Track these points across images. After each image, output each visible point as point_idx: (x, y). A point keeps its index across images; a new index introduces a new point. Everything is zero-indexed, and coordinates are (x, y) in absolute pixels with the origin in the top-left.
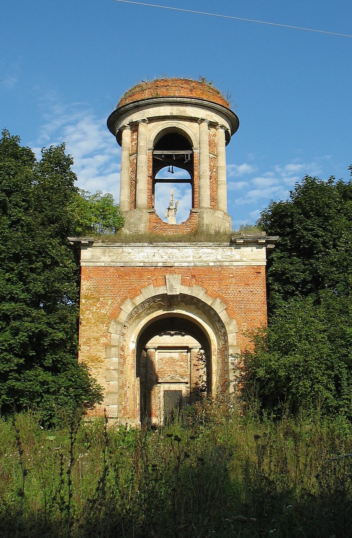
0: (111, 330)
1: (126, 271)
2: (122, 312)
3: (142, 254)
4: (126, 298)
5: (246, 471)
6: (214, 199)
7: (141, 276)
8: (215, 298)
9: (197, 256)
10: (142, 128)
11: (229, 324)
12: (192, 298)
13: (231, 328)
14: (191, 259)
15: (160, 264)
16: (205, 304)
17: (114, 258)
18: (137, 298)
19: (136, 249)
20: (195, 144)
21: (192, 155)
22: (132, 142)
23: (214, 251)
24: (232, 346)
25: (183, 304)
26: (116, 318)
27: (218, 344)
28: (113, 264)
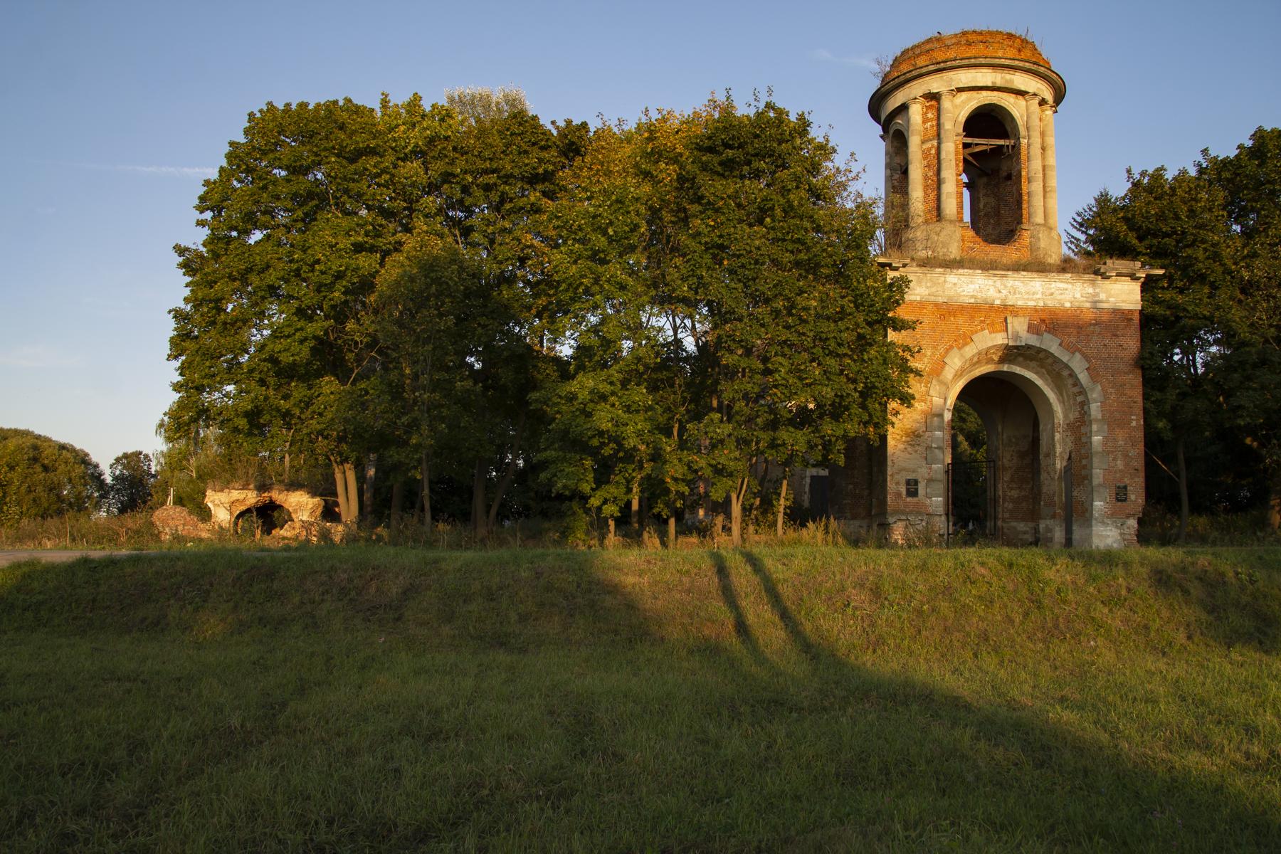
0: (932, 392)
1: (949, 310)
2: (947, 368)
3: (972, 286)
4: (951, 347)
5: (827, 527)
6: (937, 212)
7: (972, 318)
8: (1072, 350)
9: (1048, 292)
10: (946, 103)
11: (1092, 390)
12: (1040, 350)
13: (1095, 394)
14: (1039, 296)
15: (998, 302)
16: (1056, 360)
17: (934, 290)
18: (967, 349)
19: (963, 279)
20: (1023, 131)
21: (1016, 147)
22: (924, 122)
23: (1070, 286)
24: (1097, 420)
25: (1021, 359)
26: (938, 375)
27: (1066, 416)
28: (932, 298)
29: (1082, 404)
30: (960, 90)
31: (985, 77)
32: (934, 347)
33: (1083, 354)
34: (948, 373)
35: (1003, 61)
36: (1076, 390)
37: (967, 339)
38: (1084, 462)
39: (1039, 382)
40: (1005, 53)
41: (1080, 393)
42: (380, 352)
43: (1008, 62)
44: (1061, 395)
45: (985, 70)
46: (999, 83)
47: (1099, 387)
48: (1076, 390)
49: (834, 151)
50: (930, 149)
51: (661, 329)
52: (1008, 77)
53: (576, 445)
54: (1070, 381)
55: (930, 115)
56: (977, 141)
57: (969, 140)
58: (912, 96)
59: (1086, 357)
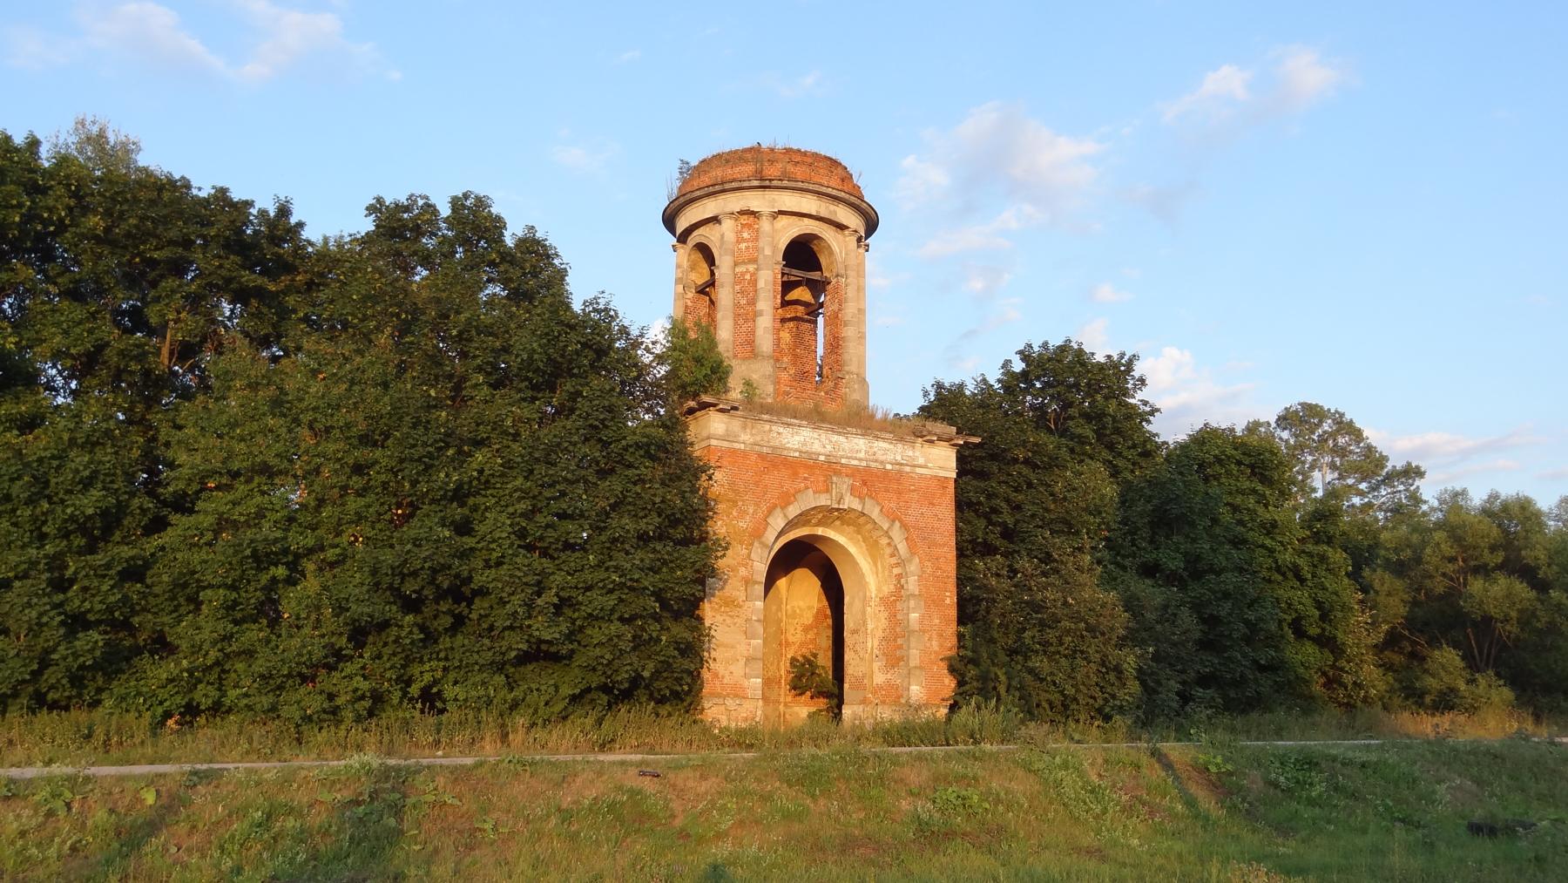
0: (753, 556)
3: (797, 438)
4: (774, 507)
17: (758, 438)
22: (738, 242)
27: (879, 589)
29: (899, 576)
30: (781, 213)
31: (809, 204)
32: (757, 505)
33: (901, 522)
34: (770, 536)
35: (829, 191)
36: (894, 560)
37: (786, 500)
38: (900, 641)
39: (852, 549)
40: (832, 184)
41: (898, 565)
42: (217, 663)
43: (834, 192)
44: (875, 564)
45: (809, 196)
46: (823, 214)
47: (917, 560)
48: (894, 560)
49: (284, 211)
50: (743, 274)
51: (11, 306)
52: (832, 208)
53: (627, 835)
54: (888, 551)
55: (745, 235)
56: (794, 272)
57: (787, 270)
58: (728, 210)
59: (904, 526)
